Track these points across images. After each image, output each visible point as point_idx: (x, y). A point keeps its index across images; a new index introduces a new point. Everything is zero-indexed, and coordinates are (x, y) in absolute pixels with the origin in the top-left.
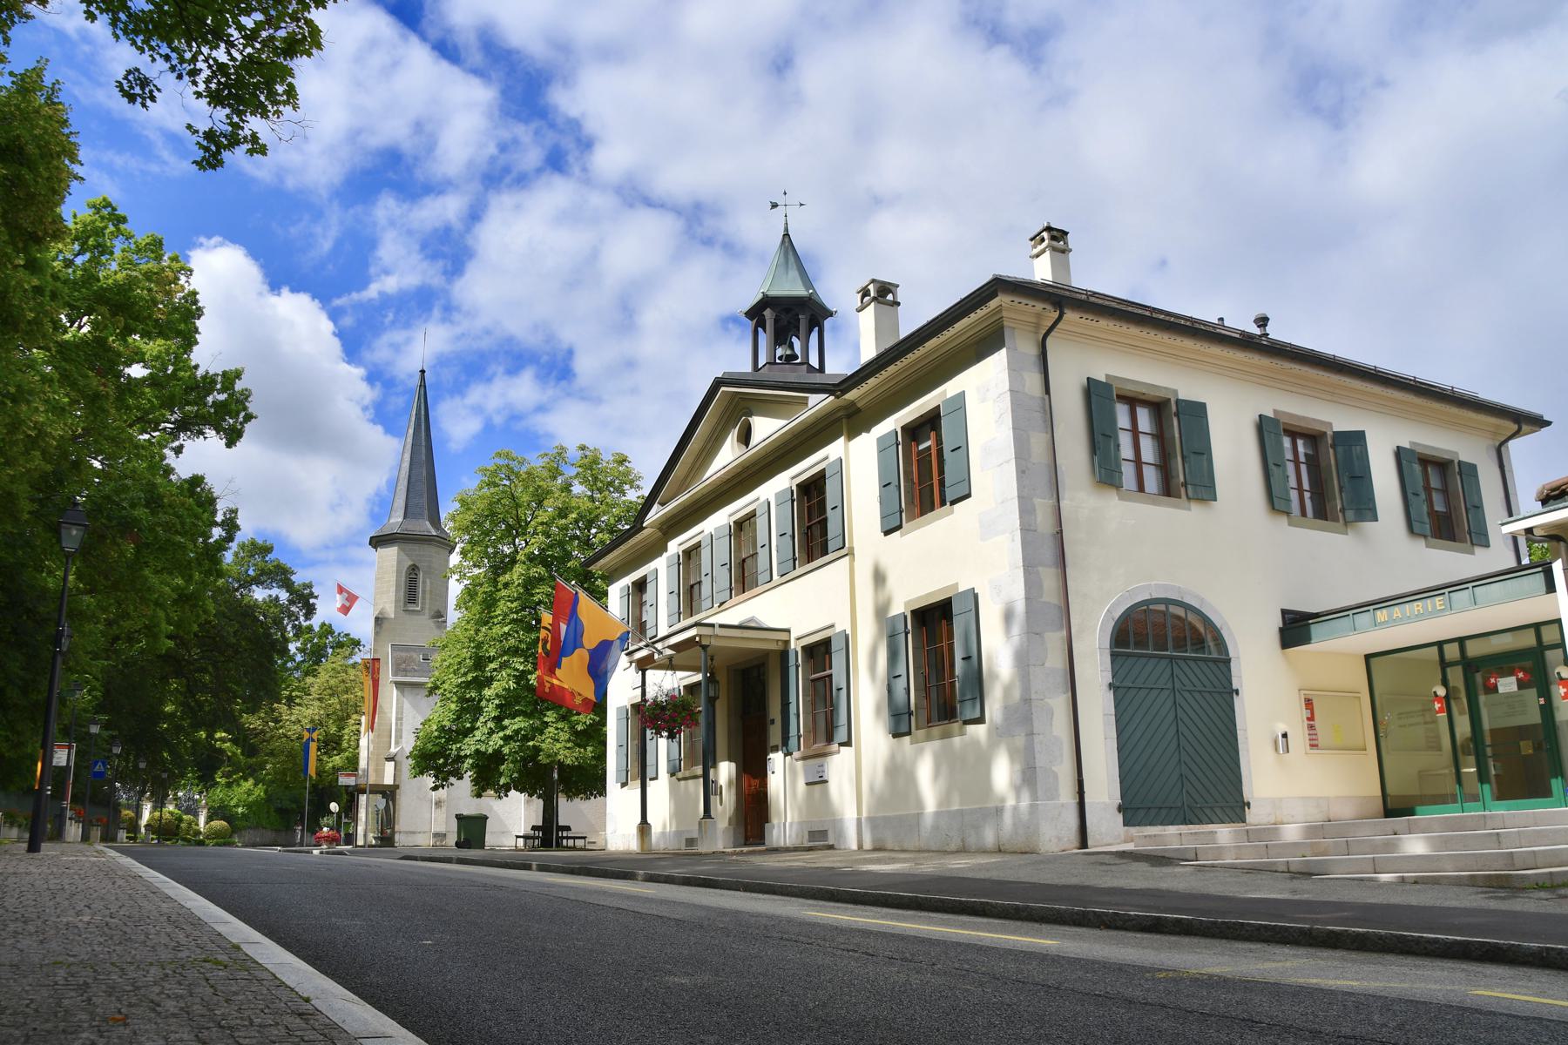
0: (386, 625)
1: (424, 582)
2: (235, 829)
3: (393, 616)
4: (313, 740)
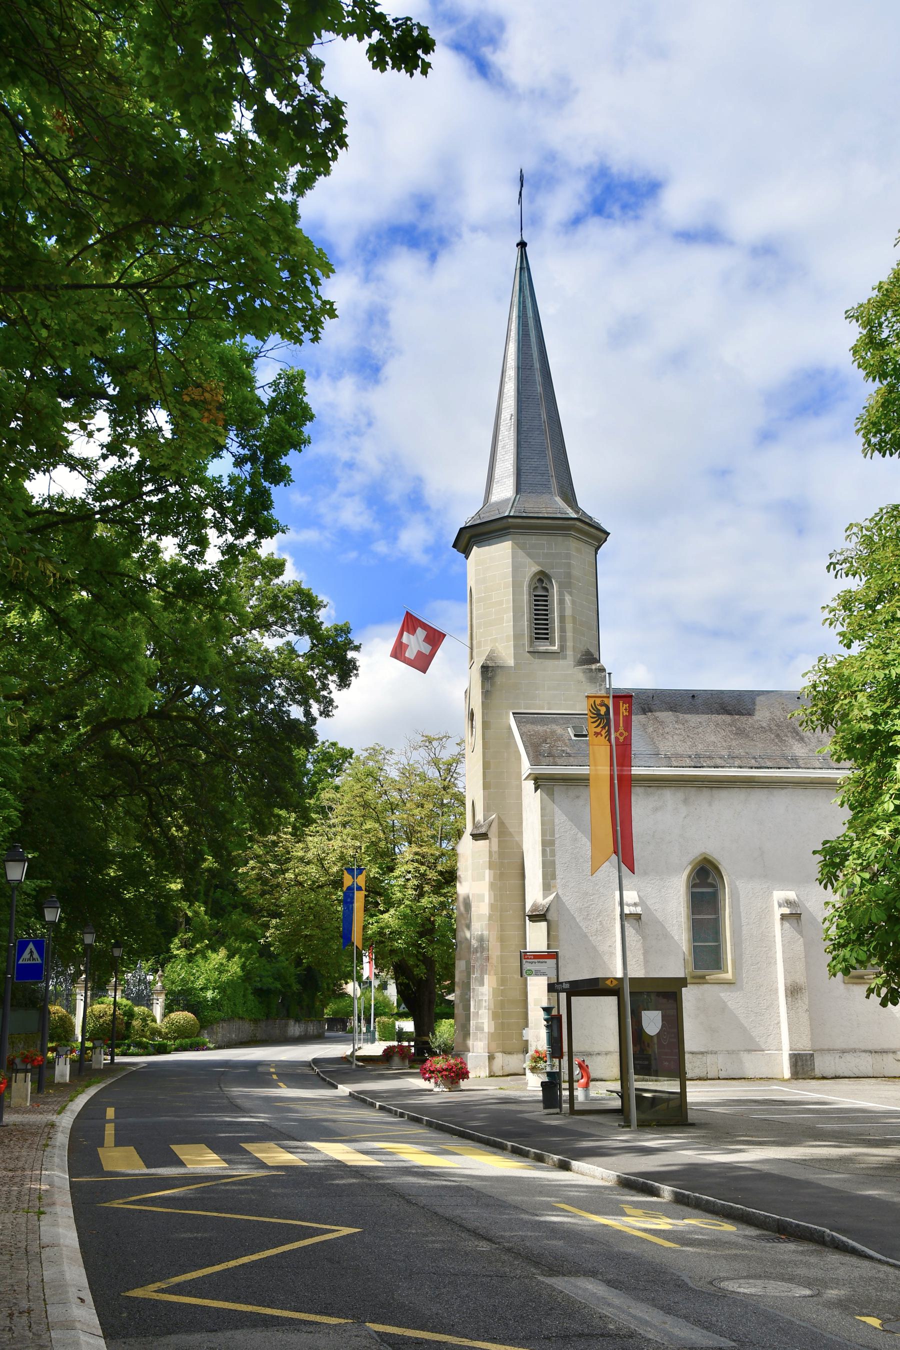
0: (500, 679)
1: (561, 602)
2: (205, 1023)
3: (511, 662)
4: (359, 889)
